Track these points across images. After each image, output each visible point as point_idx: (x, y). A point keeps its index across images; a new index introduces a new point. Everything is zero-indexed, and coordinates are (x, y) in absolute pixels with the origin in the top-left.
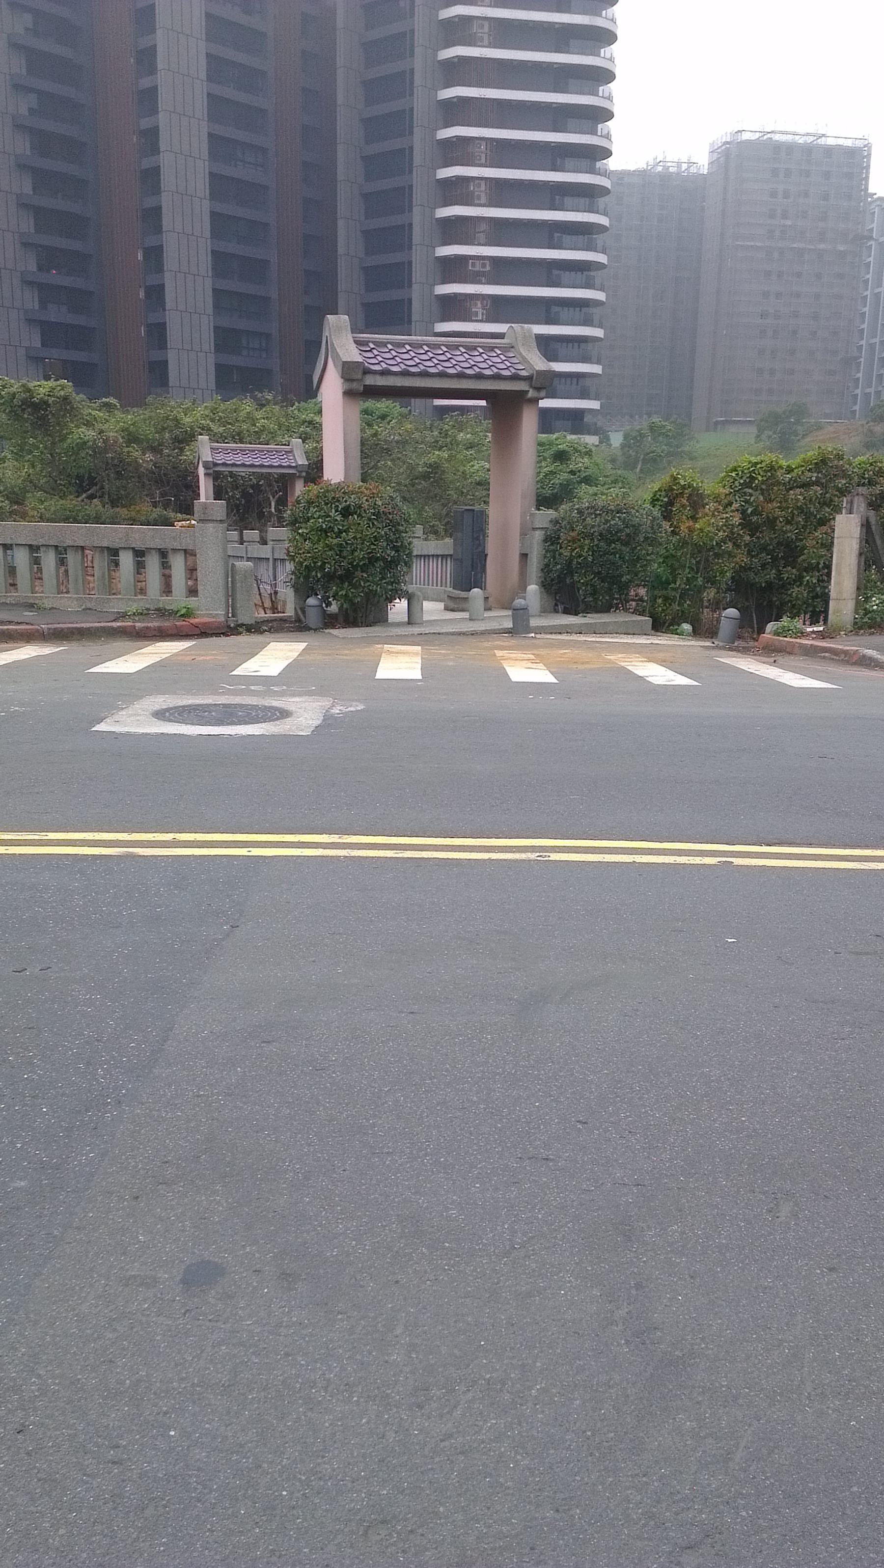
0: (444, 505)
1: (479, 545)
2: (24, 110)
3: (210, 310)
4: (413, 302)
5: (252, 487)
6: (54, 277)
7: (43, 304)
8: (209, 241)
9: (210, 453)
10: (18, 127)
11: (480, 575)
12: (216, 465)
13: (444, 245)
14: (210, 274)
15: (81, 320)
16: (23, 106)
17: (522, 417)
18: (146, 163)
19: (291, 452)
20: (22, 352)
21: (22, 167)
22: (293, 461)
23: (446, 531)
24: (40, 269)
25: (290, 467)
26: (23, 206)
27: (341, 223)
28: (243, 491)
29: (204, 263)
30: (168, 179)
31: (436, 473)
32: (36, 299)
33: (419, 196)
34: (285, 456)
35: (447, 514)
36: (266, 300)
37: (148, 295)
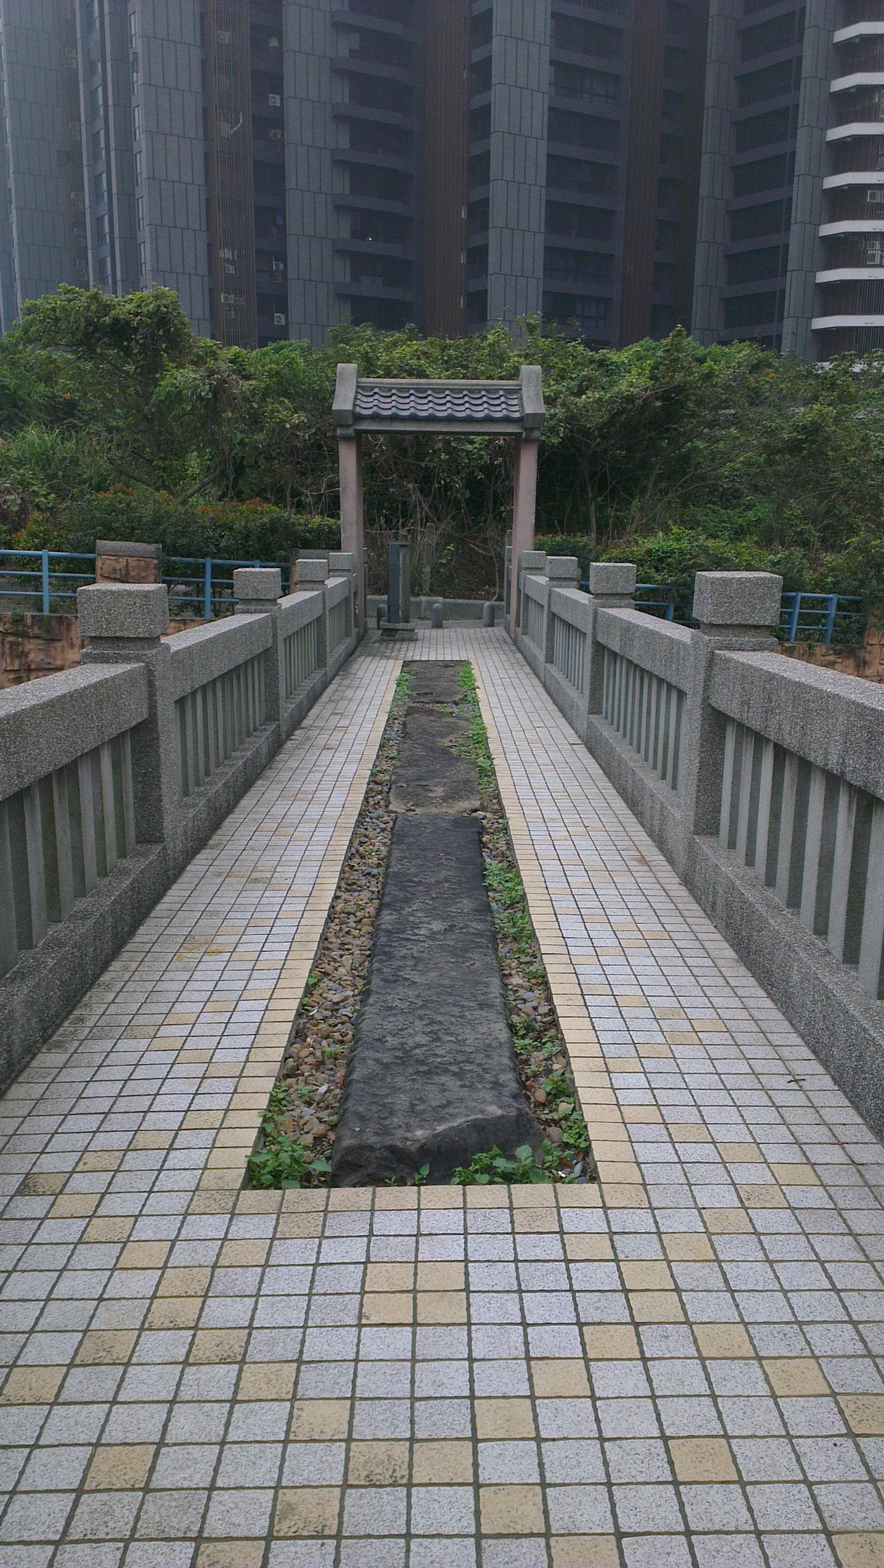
0: (823, 497)
2: (343, 52)
3: (540, 273)
4: (790, 247)
5: (484, 469)
7: (356, 277)
8: (543, 189)
9: (352, 396)
10: (338, 72)
12: (358, 418)
13: (842, 124)
14: (542, 229)
16: (344, 46)
18: (477, 102)
19: (517, 391)
21: (338, 118)
23: (823, 540)
24: (355, 235)
25: (507, 420)
26: (338, 163)
27: (705, 159)
29: (536, 216)
30: (499, 118)
31: (813, 442)
32: (348, 272)
33: (792, 302)
34: (503, 399)
35: (827, 512)
37: (470, 260)
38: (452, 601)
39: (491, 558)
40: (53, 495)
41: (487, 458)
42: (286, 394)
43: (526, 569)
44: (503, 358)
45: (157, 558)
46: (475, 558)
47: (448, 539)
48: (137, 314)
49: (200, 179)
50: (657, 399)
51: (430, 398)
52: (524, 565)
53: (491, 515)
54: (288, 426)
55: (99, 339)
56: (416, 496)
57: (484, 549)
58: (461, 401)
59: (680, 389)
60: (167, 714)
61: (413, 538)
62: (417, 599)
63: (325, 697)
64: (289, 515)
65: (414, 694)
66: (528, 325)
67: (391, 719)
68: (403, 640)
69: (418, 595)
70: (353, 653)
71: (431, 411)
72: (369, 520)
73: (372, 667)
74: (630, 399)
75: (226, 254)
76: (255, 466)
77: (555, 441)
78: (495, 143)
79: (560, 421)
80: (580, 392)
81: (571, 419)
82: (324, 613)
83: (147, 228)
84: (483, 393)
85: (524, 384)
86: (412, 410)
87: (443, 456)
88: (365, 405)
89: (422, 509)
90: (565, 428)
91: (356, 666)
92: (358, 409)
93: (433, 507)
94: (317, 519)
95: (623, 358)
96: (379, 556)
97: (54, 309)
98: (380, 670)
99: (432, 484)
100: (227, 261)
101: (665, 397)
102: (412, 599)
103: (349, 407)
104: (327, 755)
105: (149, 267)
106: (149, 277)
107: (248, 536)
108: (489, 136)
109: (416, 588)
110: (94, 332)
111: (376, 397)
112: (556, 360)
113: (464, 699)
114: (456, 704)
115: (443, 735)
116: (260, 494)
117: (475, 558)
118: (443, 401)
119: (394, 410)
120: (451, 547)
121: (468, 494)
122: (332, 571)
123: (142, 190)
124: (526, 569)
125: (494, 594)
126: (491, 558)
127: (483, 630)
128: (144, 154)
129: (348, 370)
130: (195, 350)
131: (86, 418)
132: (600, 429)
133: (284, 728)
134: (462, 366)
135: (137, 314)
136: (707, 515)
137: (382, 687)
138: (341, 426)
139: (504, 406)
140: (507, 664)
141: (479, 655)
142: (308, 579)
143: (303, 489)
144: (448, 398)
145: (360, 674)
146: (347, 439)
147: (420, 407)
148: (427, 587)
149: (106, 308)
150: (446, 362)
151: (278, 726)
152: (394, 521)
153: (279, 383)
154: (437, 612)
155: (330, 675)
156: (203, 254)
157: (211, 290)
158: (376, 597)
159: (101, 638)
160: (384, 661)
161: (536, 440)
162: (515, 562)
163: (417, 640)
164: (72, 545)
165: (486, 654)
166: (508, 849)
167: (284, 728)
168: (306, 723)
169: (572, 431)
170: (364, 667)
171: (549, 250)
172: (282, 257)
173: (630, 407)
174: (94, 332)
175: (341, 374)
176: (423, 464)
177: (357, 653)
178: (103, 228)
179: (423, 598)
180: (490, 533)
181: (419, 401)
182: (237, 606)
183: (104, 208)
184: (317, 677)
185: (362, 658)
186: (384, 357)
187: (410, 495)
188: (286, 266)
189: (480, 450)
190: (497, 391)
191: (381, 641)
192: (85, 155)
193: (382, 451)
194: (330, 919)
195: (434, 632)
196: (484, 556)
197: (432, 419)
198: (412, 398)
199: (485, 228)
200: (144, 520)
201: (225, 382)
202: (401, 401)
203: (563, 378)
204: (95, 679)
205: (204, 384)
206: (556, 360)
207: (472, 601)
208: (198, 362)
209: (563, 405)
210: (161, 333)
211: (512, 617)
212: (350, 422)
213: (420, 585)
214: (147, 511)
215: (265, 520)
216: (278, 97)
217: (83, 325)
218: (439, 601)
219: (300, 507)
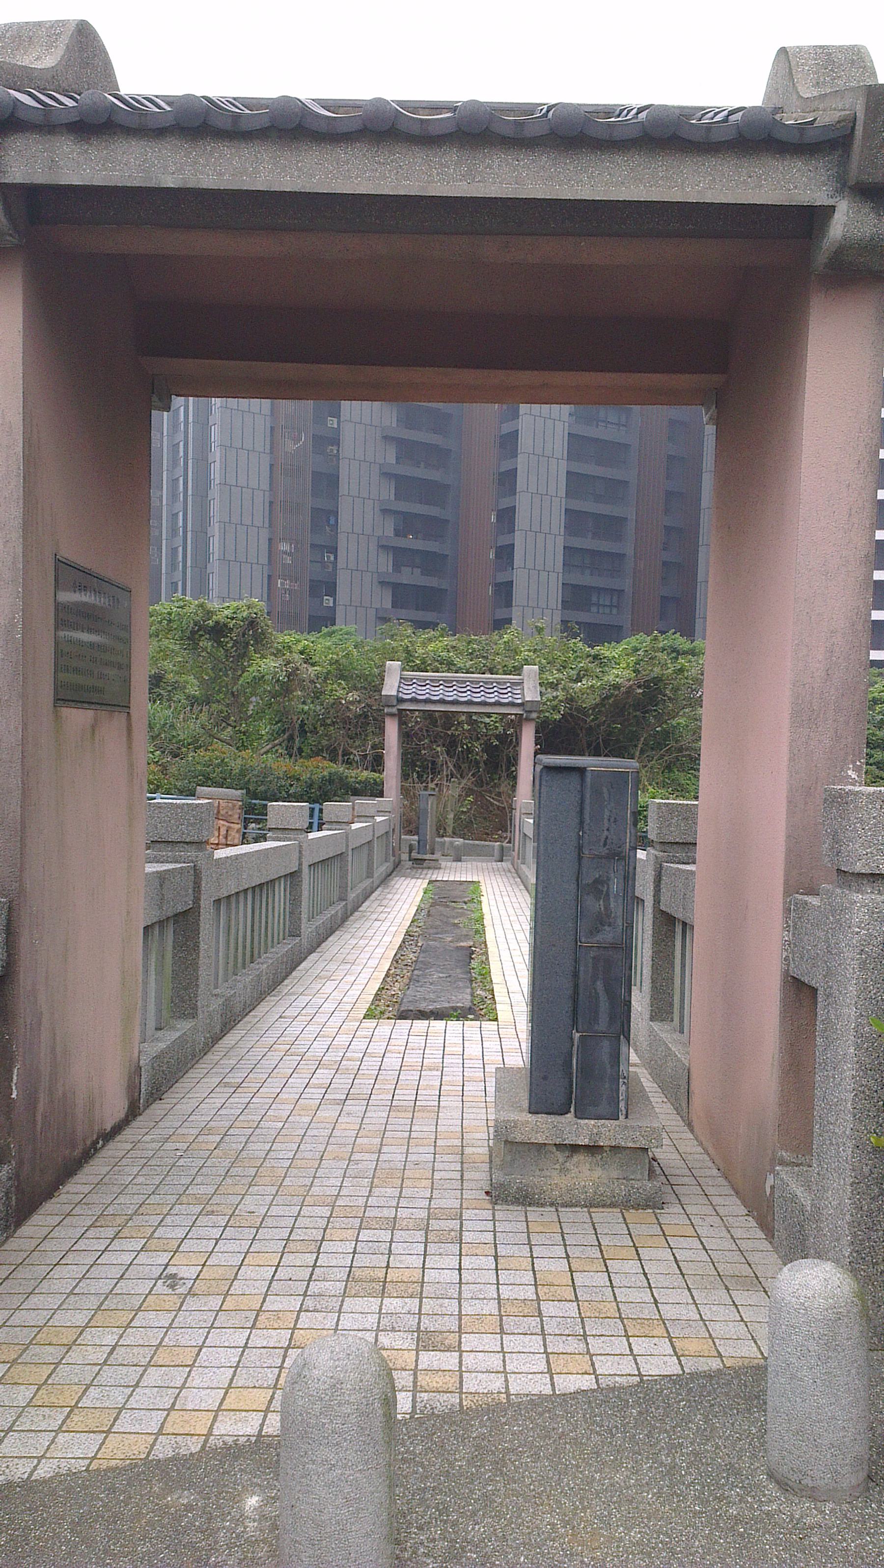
1: (602, 920)
5: (497, 737)
6: (410, 542)
7: (397, 567)
8: (563, 500)
9: (397, 684)
11: (606, 1045)
12: (401, 701)
15: (432, 582)
17: (803, 358)
20: (372, 613)
22: (519, 696)
24: (397, 533)
25: (512, 704)
28: (486, 743)
29: (557, 521)
34: (509, 689)
36: (621, 556)
38: (471, 842)
39: (504, 808)
40: (158, 752)
41: (501, 729)
42: (342, 677)
43: (524, 814)
44: (516, 652)
45: (242, 801)
46: (491, 808)
47: (469, 792)
48: (232, 618)
49: (265, 486)
50: (639, 687)
51: (455, 687)
52: (523, 811)
53: (504, 774)
54: (344, 702)
55: (202, 636)
56: (443, 758)
57: (499, 801)
58: (478, 690)
59: (657, 680)
60: (305, 869)
61: (439, 791)
62: (442, 840)
63: (372, 898)
64: (340, 768)
65: (436, 897)
66: (536, 627)
67: (419, 910)
68: (429, 868)
69: (443, 836)
70: (390, 875)
71: (455, 697)
72: (405, 776)
73: (406, 882)
74: (617, 687)
75: (284, 547)
76: (315, 731)
77: (558, 717)
78: (521, 463)
79: (561, 701)
80: (579, 679)
81: (570, 700)
82: (373, 839)
83: (217, 525)
84: (495, 684)
85: (525, 678)
86: (441, 696)
87: (466, 727)
88: (406, 692)
89: (448, 767)
90: (566, 707)
91: (393, 882)
92: (400, 694)
93: (457, 767)
94: (365, 773)
95: (614, 654)
96: (412, 804)
97: (170, 614)
98: (411, 885)
99: (457, 747)
100: (285, 553)
101: (646, 685)
102: (438, 839)
103: (394, 693)
104: (378, 924)
105: (216, 556)
106: (217, 564)
107: (311, 785)
108: (517, 456)
109: (441, 830)
110: (198, 630)
111: (414, 686)
112: (559, 654)
113: (472, 901)
114: (466, 903)
115: (454, 917)
116: (317, 753)
117: (491, 808)
118: (465, 690)
119: (427, 695)
120: (471, 798)
121: (485, 756)
122: (380, 812)
123: (215, 493)
124: (524, 814)
125: (506, 838)
126: (504, 808)
127: (494, 863)
128: (218, 464)
129: (394, 666)
130: (276, 645)
131: (170, 688)
132: (594, 709)
133: (349, 907)
134: (484, 657)
135: (232, 618)
136: (690, 779)
137: (413, 894)
138: (389, 706)
139: (510, 694)
140: (507, 884)
141: (487, 878)
142: (363, 814)
143: (352, 750)
144: (469, 688)
145: (397, 886)
146: (392, 715)
147: (447, 694)
148: (450, 830)
149: (209, 614)
150: (471, 654)
151: (346, 904)
152: (425, 776)
153: (338, 669)
154: (457, 849)
155: (375, 885)
156: (264, 546)
157: (269, 577)
158: (408, 837)
159: (278, 829)
160: (414, 881)
161: (533, 719)
162: (518, 810)
163: (440, 868)
164: (179, 790)
165: (493, 878)
166: (486, 959)
167: (349, 907)
168: (361, 909)
169: (571, 709)
170: (400, 882)
171: (568, 550)
172: (334, 550)
173: (616, 693)
174: (198, 630)
175: (389, 669)
176: (449, 732)
177: (393, 875)
178: (177, 523)
179: (446, 839)
180: (503, 788)
181: (447, 689)
182: (324, 826)
183: (179, 506)
184: (367, 883)
185: (398, 878)
186: (421, 651)
187: (439, 756)
188: (336, 558)
189: (496, 722)
190: (505, 683)
191: (412, 868)
192: (165, 462)
193: (417, 722)
194: (387, 976)
195: (454, 864)
196: (498, 807)
197: (455, 703)
198: (441, 687)
199: (512, 530)
200: (234, 772)
201: (298, 669)
202: (433, 689)
203: (564, 667)
204: (275, 845)
205: (282, 671)
206: (559, 654)
207: (487, 843)
208: (277, 654)
209: (563, 689)
210: (251, 632)
211: (515, 854)
212: (395, 704)
213: (445, 829)
214: (236, 765)
215: (325, 773)
216: (335, 420)
217: (191, 625)
218: (459, 841)
219: (349, 763)
